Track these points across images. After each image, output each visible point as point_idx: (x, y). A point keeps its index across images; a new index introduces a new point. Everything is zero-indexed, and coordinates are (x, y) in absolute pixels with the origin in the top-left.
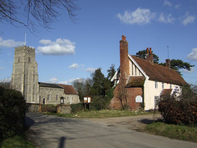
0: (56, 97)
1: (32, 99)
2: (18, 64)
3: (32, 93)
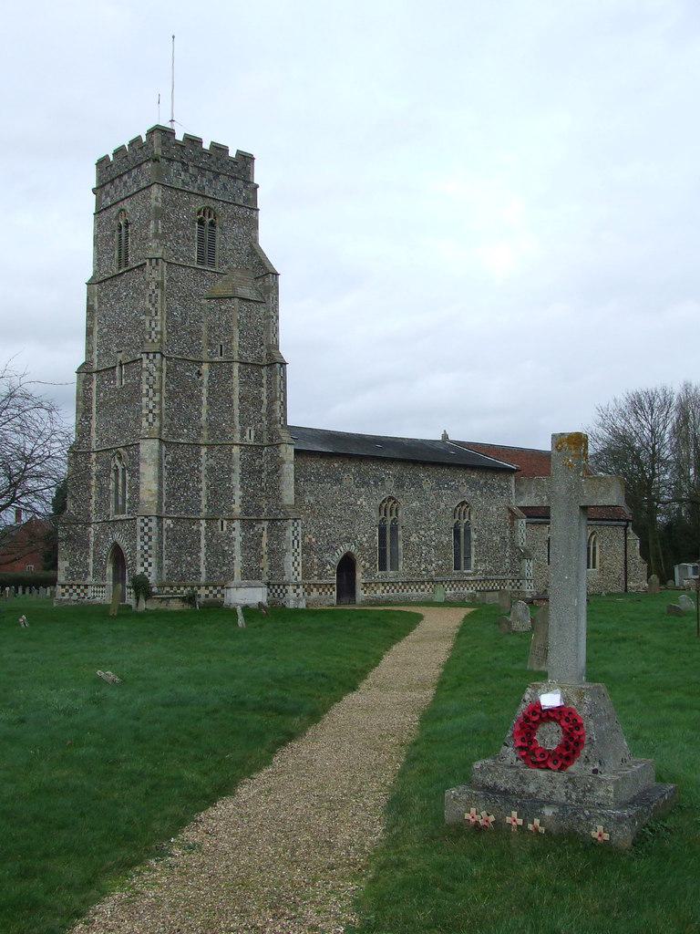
0: (448, 539)
1: (238, 558)
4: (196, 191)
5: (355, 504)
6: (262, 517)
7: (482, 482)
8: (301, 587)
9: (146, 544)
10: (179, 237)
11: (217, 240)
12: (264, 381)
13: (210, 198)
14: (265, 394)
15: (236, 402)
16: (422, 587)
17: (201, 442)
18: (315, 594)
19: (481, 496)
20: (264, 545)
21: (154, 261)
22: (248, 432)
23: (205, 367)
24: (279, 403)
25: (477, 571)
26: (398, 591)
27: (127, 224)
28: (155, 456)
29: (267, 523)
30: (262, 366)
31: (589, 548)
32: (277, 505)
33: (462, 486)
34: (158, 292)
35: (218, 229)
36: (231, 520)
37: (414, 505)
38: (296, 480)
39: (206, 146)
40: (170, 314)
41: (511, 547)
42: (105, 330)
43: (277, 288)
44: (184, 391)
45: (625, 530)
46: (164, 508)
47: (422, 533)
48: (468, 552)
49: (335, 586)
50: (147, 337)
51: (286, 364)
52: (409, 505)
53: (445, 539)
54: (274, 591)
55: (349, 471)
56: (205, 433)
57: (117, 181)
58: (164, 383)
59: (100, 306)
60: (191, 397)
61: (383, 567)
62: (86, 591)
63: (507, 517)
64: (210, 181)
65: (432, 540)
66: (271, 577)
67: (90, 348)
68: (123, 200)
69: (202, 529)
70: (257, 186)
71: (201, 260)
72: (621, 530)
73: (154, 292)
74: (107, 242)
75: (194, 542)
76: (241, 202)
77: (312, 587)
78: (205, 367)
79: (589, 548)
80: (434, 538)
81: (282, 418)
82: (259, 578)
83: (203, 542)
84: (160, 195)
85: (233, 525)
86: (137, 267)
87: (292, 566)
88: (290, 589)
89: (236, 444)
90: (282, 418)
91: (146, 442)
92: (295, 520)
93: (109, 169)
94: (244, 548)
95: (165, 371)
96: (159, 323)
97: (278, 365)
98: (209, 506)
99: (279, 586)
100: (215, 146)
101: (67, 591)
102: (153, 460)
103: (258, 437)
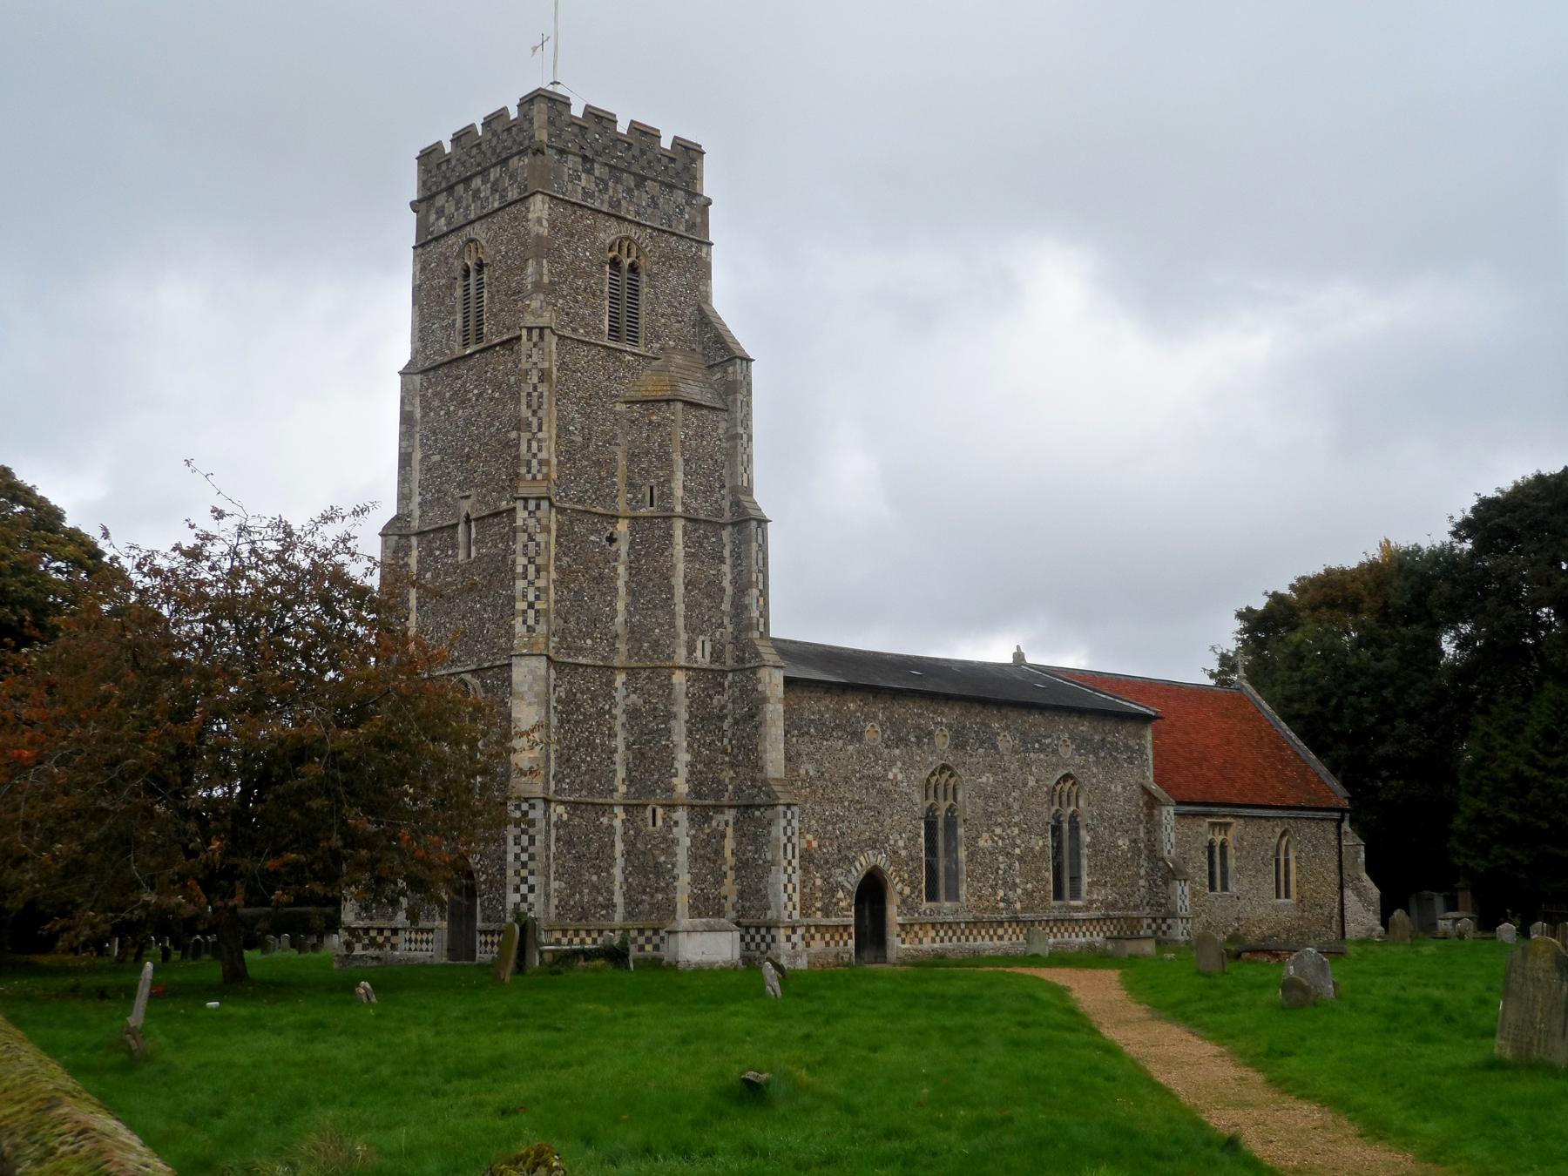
0: (1041, 843)
1: (684, 879)
4: (605, 209)
5: (884, 778)
7: (1097, 738)
9: (524, 850)
11: (642, 297)
12: (726, 553)
13: (630, 221)
14: (729, 577)
15: (680, 590)
16: (1000, 931)
17: (616, 663)
19: (1097, 763)
20: (728, 853)
21: (536, 333)
23: (622, 527)
24: (755, 592)
26: (959, 940)
27: (480, 266)
28: (540, 687)
30: (723, 526)
31: (1277, 862)
32: (753, 780)
33: (1064, 738)
35: (644, 278)
36: (671, 807)
37: (984, 779)
38: (786, 733)
39: (622, 128)
40: (563, 430)
41: (1149, 858)
42: (437, 458)
43: (749, 384)
44: (587, 569)
45: (1339, 827)
46: (552, 784)
47: (998, 831)
48: (1076, 867)
49: (852, 930)
53: (1038, 844)
54: (758, 938)
55: (875, 717)
56: (622, 647)
57: (460, 189)
62: (394, 940)
63: (1141, 804)
64: (629, 191)
65: (1014, 845)
66: (743, 912)
67: (406, 491)
68: (472, 222)
69: (617, 823)
70: (709, 203)
71: (615, 332)
72: (1331, 827)
73: (535, 389)
75: (602, 847)
76: (681, 229)
78: (622, 527)
79: (1277, 862)
80: (1018, 842)
81: (762, 620)
82: (720, 913)
83: (619, 847)
84: (545, 214)
86: (502, 344)
88: (781, 934)
89: (680, 668)
90: (762, 620)
91: (524, 662)
92: (788, 806)
93: (444, 167)
94: (694, 858)
95: (554, 533)
97: (754, 524)
98: (629, 780)
99: (758, 929)
102: (537, 695)
103: (717, 655)
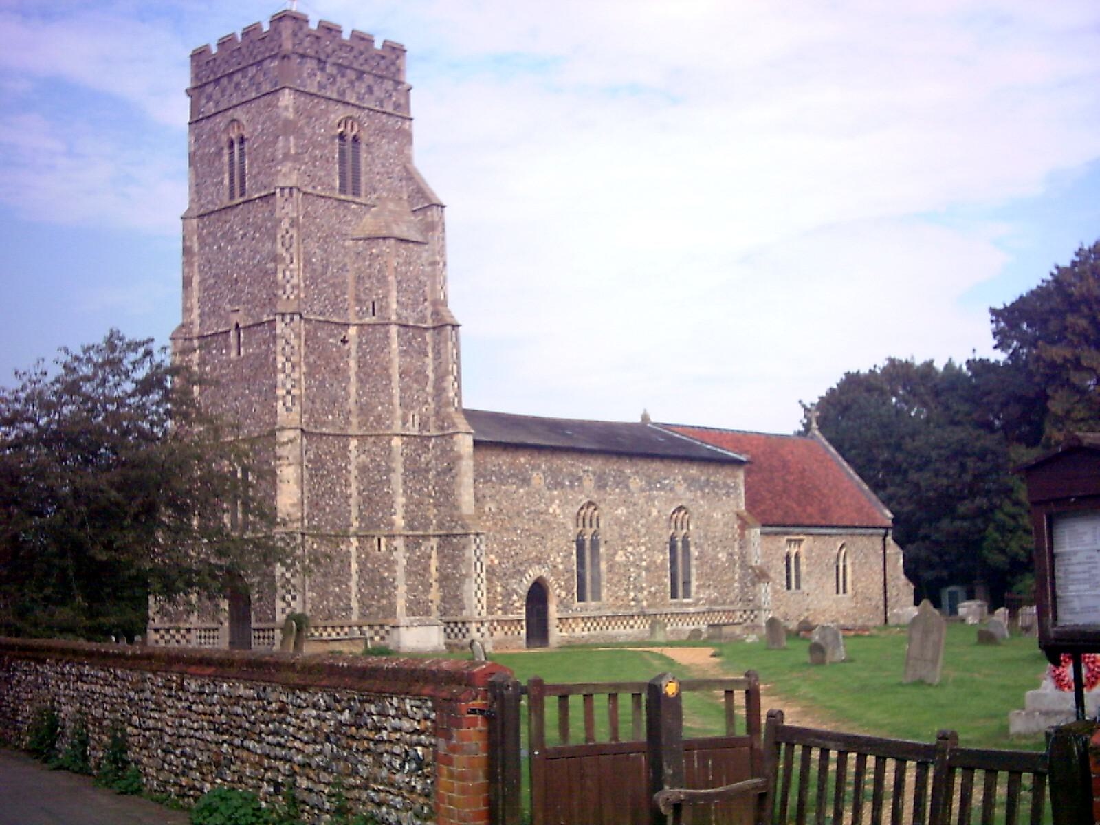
0: (662, 557)
1: (402, 589)
2: (234, 218)
3: (399, 521)
4: (335, 96)
5: (546, 512)
6: (431, 532)
7: (703, 478)
8: (486, 625)
10: (314, 159)
13: (353, 105)
16: (631, 622)
17: (350, 432)
18: (499, 634)
19: (703, 497)
20: (433, 569)
21: (287, 191)
22: (411, 419)
23: (353, 331)
24: (451, 378)
25: (699, 600)
27: (242, 140)
29: (437, 539)
31: (838, 567)
32: (452, 516)
34: (293, 232)
36: (391, 537)
40: (308, 262)
41: (741, 567)
45: (884, 540)
47: (630, 549)
48: (687, 574)
49: (524, 623)
50: (280, 292)
51: (458, 326)
52: (613, 512)
53: (659, 558)
54: (456, 630)
56: (354, 420)
57: (225, 81)
58: (303, 354)
59: (201, 248)
60: (337, 370)
61: (581, 598)
63: (736, 526)
64: (352, 83)
68: (234, 107)
69: (353, 549)
71: (342, 189)
72: (879, 541)
74: (211, 164)
75: (342, 568)
76: (390, 110)
77: (495, 624)
78: (353, 331)
81: (456, 400)
83: (354, 566)
85: (395, 543)
86: (260, 198)
87: (475, 596)
88: (473, 627)
89: (397, 435)
94: (409, 574)
95: (303, 338)
96: (295, 273)
97: (449, 328)
98: (361, 518)
100: (356, 35)
101: (162, 637)
103: (423, 425)
